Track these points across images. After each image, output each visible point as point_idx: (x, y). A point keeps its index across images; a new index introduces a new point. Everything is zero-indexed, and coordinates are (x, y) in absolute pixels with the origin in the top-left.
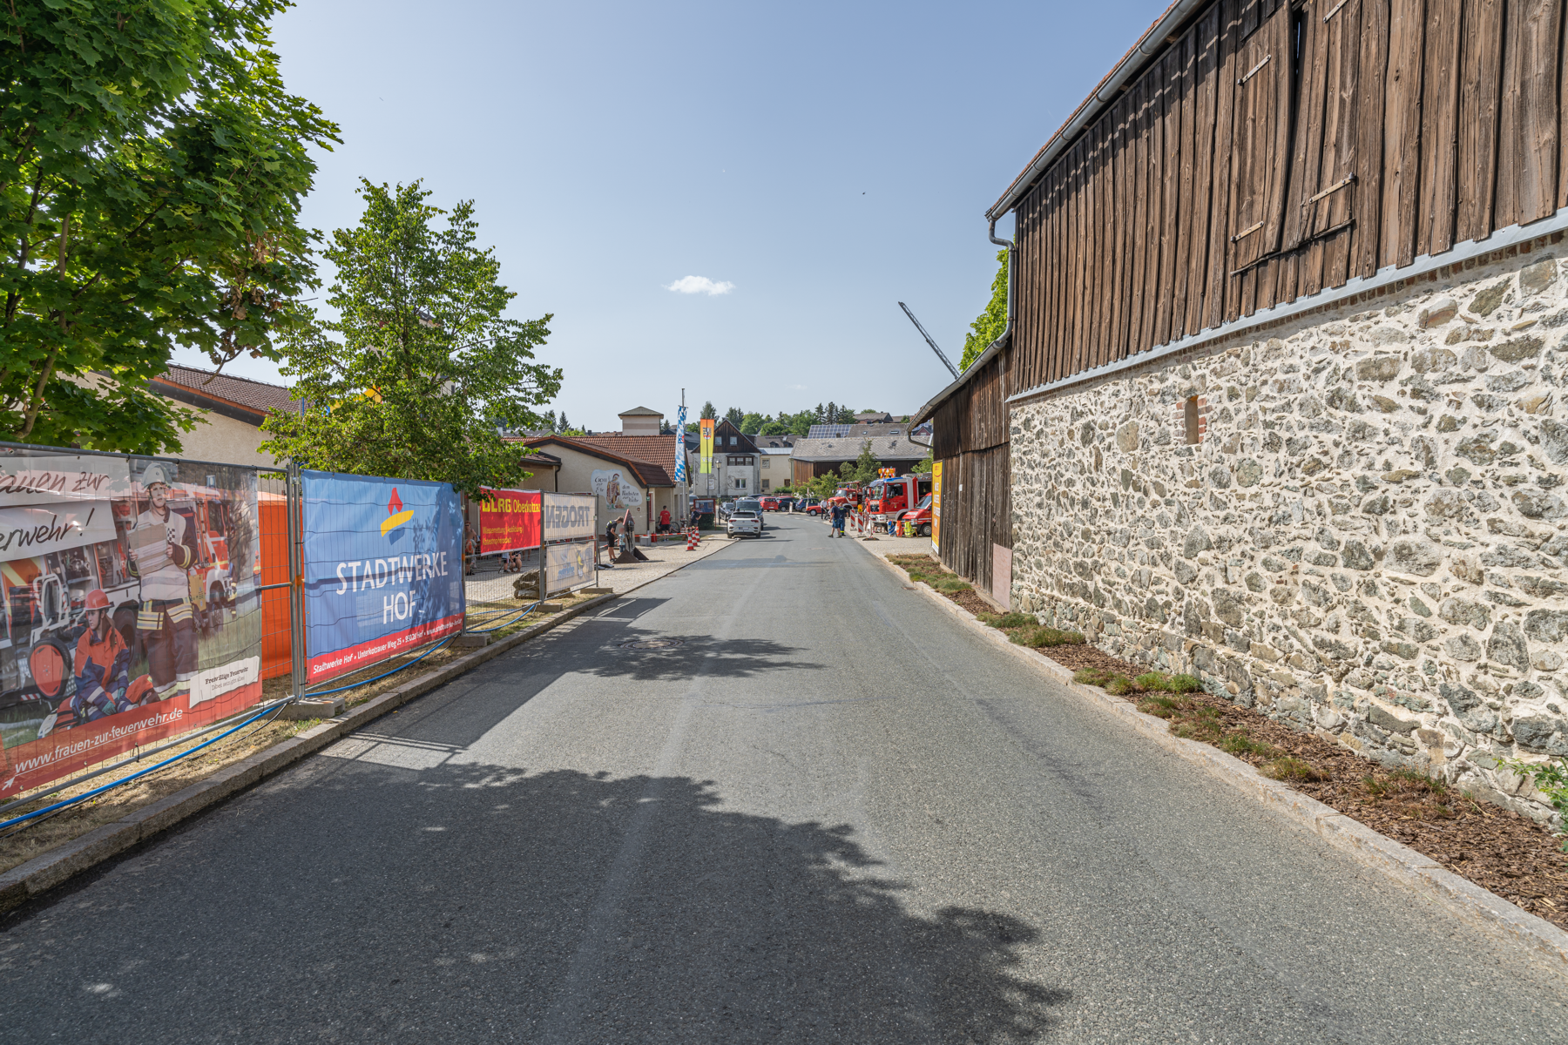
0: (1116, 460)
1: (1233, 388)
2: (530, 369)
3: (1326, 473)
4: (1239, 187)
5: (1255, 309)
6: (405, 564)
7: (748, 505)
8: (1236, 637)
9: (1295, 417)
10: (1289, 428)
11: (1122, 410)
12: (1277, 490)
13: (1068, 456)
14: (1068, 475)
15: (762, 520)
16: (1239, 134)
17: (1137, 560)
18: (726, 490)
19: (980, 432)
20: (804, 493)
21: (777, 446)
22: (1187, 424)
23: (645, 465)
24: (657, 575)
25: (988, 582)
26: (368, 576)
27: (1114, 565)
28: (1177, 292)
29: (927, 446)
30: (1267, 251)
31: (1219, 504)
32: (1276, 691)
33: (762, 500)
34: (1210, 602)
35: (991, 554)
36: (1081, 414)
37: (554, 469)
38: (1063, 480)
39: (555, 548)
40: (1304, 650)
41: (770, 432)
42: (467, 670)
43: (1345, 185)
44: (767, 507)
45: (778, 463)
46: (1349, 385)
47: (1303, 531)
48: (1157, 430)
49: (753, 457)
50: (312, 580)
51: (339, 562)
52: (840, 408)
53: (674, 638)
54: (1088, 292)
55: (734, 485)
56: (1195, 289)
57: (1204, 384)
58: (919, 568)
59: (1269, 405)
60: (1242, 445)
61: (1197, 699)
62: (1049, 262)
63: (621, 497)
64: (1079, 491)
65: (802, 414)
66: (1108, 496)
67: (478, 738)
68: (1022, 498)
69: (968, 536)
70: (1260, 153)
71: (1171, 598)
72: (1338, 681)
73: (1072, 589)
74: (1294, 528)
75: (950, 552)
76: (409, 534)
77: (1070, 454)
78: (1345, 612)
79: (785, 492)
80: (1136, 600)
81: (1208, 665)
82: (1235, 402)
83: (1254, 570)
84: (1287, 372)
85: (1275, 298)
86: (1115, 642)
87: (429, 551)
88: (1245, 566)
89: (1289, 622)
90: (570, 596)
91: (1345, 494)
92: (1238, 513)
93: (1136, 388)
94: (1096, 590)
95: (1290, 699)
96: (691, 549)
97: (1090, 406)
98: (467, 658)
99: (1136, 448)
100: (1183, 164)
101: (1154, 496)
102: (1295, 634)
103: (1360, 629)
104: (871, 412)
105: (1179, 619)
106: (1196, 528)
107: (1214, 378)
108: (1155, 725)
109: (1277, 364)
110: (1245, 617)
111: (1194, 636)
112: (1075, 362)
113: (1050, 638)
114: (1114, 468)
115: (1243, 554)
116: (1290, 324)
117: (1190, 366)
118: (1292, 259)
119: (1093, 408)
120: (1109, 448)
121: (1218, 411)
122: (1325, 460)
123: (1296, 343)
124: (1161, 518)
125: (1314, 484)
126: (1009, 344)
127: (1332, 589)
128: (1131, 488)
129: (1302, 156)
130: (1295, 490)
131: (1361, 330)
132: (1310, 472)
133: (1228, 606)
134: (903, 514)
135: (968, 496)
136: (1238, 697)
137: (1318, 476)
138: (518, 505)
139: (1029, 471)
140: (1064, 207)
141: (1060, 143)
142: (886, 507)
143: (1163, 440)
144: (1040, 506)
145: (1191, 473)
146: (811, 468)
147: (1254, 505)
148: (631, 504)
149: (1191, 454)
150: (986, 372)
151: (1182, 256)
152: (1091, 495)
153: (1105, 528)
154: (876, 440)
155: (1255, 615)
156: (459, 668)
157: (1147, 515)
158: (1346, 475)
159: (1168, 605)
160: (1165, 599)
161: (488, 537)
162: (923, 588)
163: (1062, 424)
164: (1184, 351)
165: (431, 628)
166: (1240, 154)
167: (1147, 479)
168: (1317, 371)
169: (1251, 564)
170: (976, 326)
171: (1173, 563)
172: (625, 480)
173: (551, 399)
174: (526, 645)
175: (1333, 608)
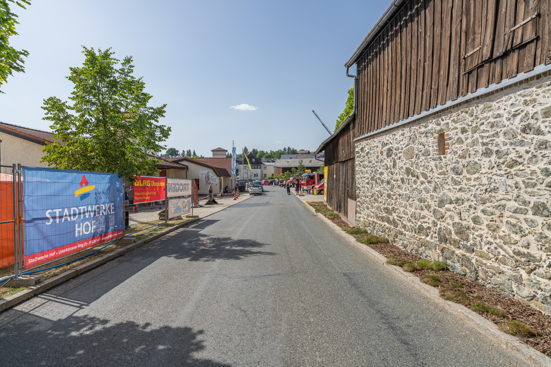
0: (403, 164)
1: (464, 128)
2: (157, 127)
3: (521, 167)
4: (466, 33)
5: (476, 89)
6: (90, 209)
7: (258, 183)
8: (466, 246)
9: (501, 139)
10: (497, 145)
11: (406, 141)
12: (490, 176)
13: (381, 162)
14: (380, 170)
15: (262, 188)
16: (466, 8)
17: (414, 207)
18: (251, 177)
19: (342, 154)
20: (278, 179)
21: (269, 162)
22: (439, 146)
23: (219, 168)
24: (219, 210)
25: (346, 214)
26: (66, 216)
27: (402, 209)
28: (433, 87)
29: (323, 161)
30: (484, 60)
31: (456, 183)
32: (490, 274)
33: (263, 181)
34: (451, 228)
35: (347, 203)
36: (386, 144)
37: (186, 170)
38: (378, 172)
39: (173, 200)
40: (507, 255)
41: (267, 157)
42: (120, 255)
43: (532, 19)
44: (265, 184)
45: (270, 168)
46: (535, 121)
47: (506, 196)
48: (423, 149)
49: (260, 166)
50: (28, 219)
51: (47, 210)
52: (292, 149)
53: (215, 239)
54: (389, 92)
55: (254, 176)
56: (443, 83)
57: (448, 127)
58: (319, 207)
59: (487, 134)
60: (469, 154)
61: (447, 274)
62: (371, 82)
63: (210, 180)
64: (385, 177)
65: (278, 151)
66: (399, 179)
67: (99, 297)
68: (360, 180)
69: (338, 195)
70: (478, 14)
71: (431, 225)
72: (529, 273)
73: (383, 219)
74: (500, 194)
75: (331, 201)
76: (92, 196)
77: (382, 161)
78: (534, 238)
79: (272, 178)
80: (413, 225)
81: (451, 258)
82: (465, 134)
83: (476, 214)
84: (496, 118)
85: (488, 82)
86: (403, 243)
87: (104, 203)
88: (471, 212)
89: (498, 241)
90: (182, 219)
91: (533, 177)
92: (467, 186)
93: (413, 131)
94: (394, 219)
95: (499, 279)
96: (235, 199)
97: (390, 140)
98: (120, 250)
99: (413, 158)
100: (435, 29)
101: (422, 179)
102: (501, 247)
103: (544, 248)
104: (303, 150)
105: (434, 235)
106: (444, 194)
107: (453, 124)
108: (432, 292)
109: (490, 114)
110: (471, 236)
111: (443, 243)
112: (383, 122)
113: (374, 240)
114: (402, 167)
115: (470, 206)
116: (498, 94)
117: (440, 119)
118: (499, 62)
119: (392, 141)
120: (400, 158)
121: (456, 139)
122: (520, 160)
123: (501, 103)
124: (425, 189)
125: (513, 173)
126: (354, 118)
127: (525, 226)
128: (410, 176)
129: (504, 10)
130: (502, 176)
131: (544, 92)
132: (511, 167)
133: (461, 231)
134: (314, 186)
135: (338, 179)
136: (468, 275)
137: (514, 169)
138: (154, 183)
139: (363, 169)
140: (378, 58)
141: (377, 29)
142: (308, 184)
143: (427, 154)
144: (368, 183)
145: (441, 168)
146: (281, 170)
147: (477, 183)
148: (214, 183)
149: (441, 159)
150: (344, 130)
151: (435, 69)
152: (391, 179)
153: (398, 193)
154: (304, 160)
155: (477, 236)
156: (115, 255)
157: (419, 188)
158: (533, 168)
159: (429, 228)
160: (428, 225)
161: (137, 196)
162: (320, 215)
163: (378, 149)
164: (437, 112)
165: (105, 236)
166: (467, 17)
167: (418, 171)
168: (515, 116)
169: (475, 211)
170: (340, 117)
171: (432, 209)
172: (212, 174)
173: (166, 140)
174: (153, 242)
175: (526, 235)
